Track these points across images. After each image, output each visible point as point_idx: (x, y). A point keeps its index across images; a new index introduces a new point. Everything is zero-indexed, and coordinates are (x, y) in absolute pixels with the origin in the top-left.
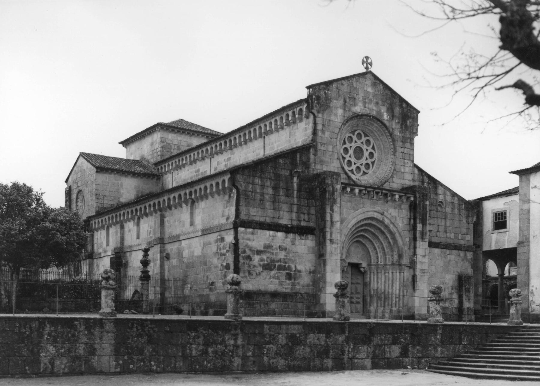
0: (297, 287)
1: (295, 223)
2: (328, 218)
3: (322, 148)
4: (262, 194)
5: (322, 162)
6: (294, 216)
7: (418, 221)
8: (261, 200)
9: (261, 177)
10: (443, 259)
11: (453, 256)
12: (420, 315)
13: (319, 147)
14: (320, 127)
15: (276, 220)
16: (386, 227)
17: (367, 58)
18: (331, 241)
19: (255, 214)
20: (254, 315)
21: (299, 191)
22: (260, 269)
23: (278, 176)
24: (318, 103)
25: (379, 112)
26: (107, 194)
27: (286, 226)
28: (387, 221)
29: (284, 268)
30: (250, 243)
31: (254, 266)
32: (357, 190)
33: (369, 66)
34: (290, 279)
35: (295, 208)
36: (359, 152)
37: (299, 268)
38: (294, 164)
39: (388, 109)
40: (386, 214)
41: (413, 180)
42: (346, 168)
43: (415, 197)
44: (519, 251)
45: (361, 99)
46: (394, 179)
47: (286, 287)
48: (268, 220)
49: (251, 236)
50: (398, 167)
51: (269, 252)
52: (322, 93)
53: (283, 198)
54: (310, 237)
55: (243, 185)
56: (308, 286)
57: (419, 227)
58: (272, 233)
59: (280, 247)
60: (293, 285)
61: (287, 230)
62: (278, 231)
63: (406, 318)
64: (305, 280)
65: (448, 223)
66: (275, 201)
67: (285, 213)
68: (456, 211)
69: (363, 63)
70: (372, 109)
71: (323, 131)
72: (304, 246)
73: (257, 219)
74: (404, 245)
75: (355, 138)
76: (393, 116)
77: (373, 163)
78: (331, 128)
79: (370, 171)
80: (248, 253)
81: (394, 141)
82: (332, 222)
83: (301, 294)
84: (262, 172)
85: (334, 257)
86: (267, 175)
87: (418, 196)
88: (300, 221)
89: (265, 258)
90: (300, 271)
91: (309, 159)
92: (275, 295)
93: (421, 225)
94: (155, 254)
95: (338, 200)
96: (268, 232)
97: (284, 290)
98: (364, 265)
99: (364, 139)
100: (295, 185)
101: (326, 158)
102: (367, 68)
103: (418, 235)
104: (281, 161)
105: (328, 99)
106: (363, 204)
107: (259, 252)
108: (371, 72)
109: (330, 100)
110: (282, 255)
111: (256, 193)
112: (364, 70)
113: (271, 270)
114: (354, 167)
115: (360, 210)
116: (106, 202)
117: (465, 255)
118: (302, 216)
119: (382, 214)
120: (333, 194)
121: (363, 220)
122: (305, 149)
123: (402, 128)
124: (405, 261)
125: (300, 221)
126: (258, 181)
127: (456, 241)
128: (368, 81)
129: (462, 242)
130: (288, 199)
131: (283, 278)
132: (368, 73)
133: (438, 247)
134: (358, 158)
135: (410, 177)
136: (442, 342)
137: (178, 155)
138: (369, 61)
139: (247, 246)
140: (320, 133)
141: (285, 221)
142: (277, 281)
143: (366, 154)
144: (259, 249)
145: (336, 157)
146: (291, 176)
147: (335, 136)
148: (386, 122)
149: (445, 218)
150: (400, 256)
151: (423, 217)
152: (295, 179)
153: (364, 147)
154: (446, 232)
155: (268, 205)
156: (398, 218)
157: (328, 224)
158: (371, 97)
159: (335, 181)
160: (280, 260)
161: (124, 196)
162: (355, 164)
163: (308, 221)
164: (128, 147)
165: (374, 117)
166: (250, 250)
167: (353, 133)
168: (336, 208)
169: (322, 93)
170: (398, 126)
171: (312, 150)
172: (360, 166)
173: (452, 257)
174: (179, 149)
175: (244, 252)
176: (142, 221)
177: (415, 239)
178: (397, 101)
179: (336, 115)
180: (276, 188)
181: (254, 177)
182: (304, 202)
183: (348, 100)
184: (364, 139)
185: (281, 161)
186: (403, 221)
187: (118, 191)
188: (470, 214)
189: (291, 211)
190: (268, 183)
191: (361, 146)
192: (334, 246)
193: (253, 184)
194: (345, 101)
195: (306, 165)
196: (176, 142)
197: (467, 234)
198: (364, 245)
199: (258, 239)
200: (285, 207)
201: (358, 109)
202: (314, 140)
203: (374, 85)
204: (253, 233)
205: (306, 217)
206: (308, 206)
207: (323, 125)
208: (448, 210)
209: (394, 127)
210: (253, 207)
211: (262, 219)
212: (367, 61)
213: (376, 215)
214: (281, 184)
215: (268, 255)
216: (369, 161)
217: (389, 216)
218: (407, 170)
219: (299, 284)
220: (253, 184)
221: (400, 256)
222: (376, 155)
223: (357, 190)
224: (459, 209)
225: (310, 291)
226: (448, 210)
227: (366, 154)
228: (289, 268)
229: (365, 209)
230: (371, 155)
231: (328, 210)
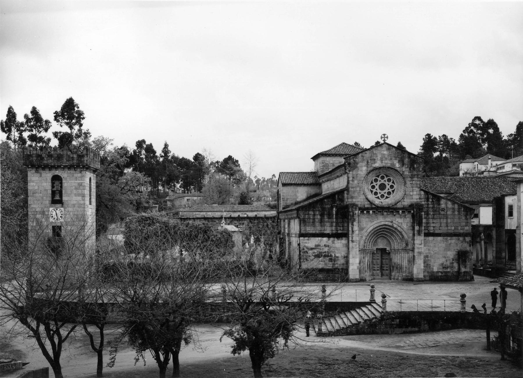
0: (336, 265)
1: (334, 232)
2: (350, 229)
3: (352, 190)
4: (314, 219)
5: (352, 198)
6: (334, 228)
7: (415, 224)
8: (313, 222)
9: (313, 211)
10: (445, 243)
11: (453, 241)
12: (417, 279)
13: (351, 189)
14: (351, 179)
15: (322, 232)
16: (396, 229)
18: (352, 241)
19: (310, 229)
21: (336, 215)
22: (313, 257)
23: (323, 209)
24: (349, 166)
25: (393, 164)
26: (289, 197)
27: (328, 234)
28: (395, 226)
29: (328, 256)
30: (306, 245)
31: (309, 256)
32: (371, 212)
33: (386, 139)
34: (331, 261)
35: (334, 224)
36: (382, 187)
37: (337, 255)
38: (334, 201)
39: (399, 161)
40: (394, 222)
41: (420, 198)
43: (414, 211)
44: (517, 232)
45: (379, 158)
46: (405, 200)
47: (330, 266)
48: (317, 232)
49: (307, 241)
50: (407, 193)
52: (352, 160)
53: (326, 220)
54: (344, 239)
55: (303, 216)
56: (343, 264)
57: (417, 228)
58: (320, 238)
59: (325, 245)
60: (334, 264)
61: (328, 236)
62: (323, 237)
65: (449, 221)
66: (321, 221)
67: (328, 228)
68: (456, 213)
70: (388, 163)
71: (353, 181)
72: (339, 244)
73: (311, 232)
74: (409, 238)
75: (379, 179)
76: (403, 164)
78: (358, 178)
79: (391, 196)
80: (306, 249)
81: (404, 178)
82: (353, 231)
83: (339, 269)
84: (314, 207)
85: (355, 250)
86: (317, 209)
87: (415, 210)
88: (337, 231)
89: (316, 251)
90: (338, 257)
91: (343, 197)
92: (321, 270)
93: (418, 227)
95: (357, 219)
96: (317, 238)
97: (328, 267)
98: (388, 249)
99: (386, 179)
100: (334, 212)
101: (356, 194)
102: (384, 140)
103: (416, 232)
104: (325, 200)
105: (356, 163)
106: (377, 218)
107: (312, 249)
109: (357, 164)
110: (326, 249)
111: (310, 219)
113: (320, 257)
115: (375, 222)
116: (288, 202)
117: (464, 239)
118: (339, 228)
119: (392, 222)
120: (353, 216)
121: (383, 225)
122: (341, 192)
123: (410, 170)
124: (410, 247)
125: (337, 231)
126: (311, 213)
127: (456, 231)
128: (385, 147)
129: (462, 231)
130: (330, 220)
131: (327, 262)
133: (441, 236)
135: (418, 197)
136: (325, 310)
137: (333, 170)
138: (386, 136)
139: (305, 246)
140: (351, 182)
141: (328, 231)
142: (324, 263)
145: (362, 193)
146: (332, 208)
147: (361, 182)
148: (398, 169)
149: (447, 218)
150: (407, 245)
151: (419, 221)
152: (334, 209)
153: (386, 183)
154: (447, 226)
155: (317, 224)
156: (403, 224)
157: (350, 232)
158: (386, 157)
159: (354, 209)
160: (325, 252)
161: (299, 198)
163: (343, 230)
164: (316, 161)
165: (389, 168)
168: (355, 223)
169: (352, 160)
170: (408, 169)
171: (345, 192)
173: (453, 241)
174: (333, 165)
175: (304, 249)
177: (414, 235)
178: (406, 155)
179: (361, 171)
180: (322, 215)
181: (309, 211)
182: (340, 220)
183: (370, 161)
184: (386, 179)
185: (325, 200)
186: (407, 225)
187: (296, 195)
188: (469, 213)
189: (332, 226)
190: (317, 213)
192: (354, 244)
193: (308, 214)
194: (368, 162)
195: (342, 200)
196: (331, 162)
197: (466, 226)
198: (386, 238)
199: (312, 242)
200: (328, 224)
201: (378, 164)
202: (347, 186)
203: (389, 149)
204: (308, 240)
205: (341, 228)
206: (343, 222)
207: (353, 178)
208: (449, 213)
209: (404, 170)
210: (308, 226)
211: (314, 232)
213: (387, 223)
214: (326, 213)
215: (317, 250)
217: (397, 223)
218: (415, 193)
219: (337, 264)
220: (308, 214)
221: (407, 245)
222: (395, 186)
223: (371, 212)
224: (459, 211)
225: (345, 268)
226: (449, 213)
228: (331, 256)
229: (378, 221)
230: (392, 187)
231: (350, 225)
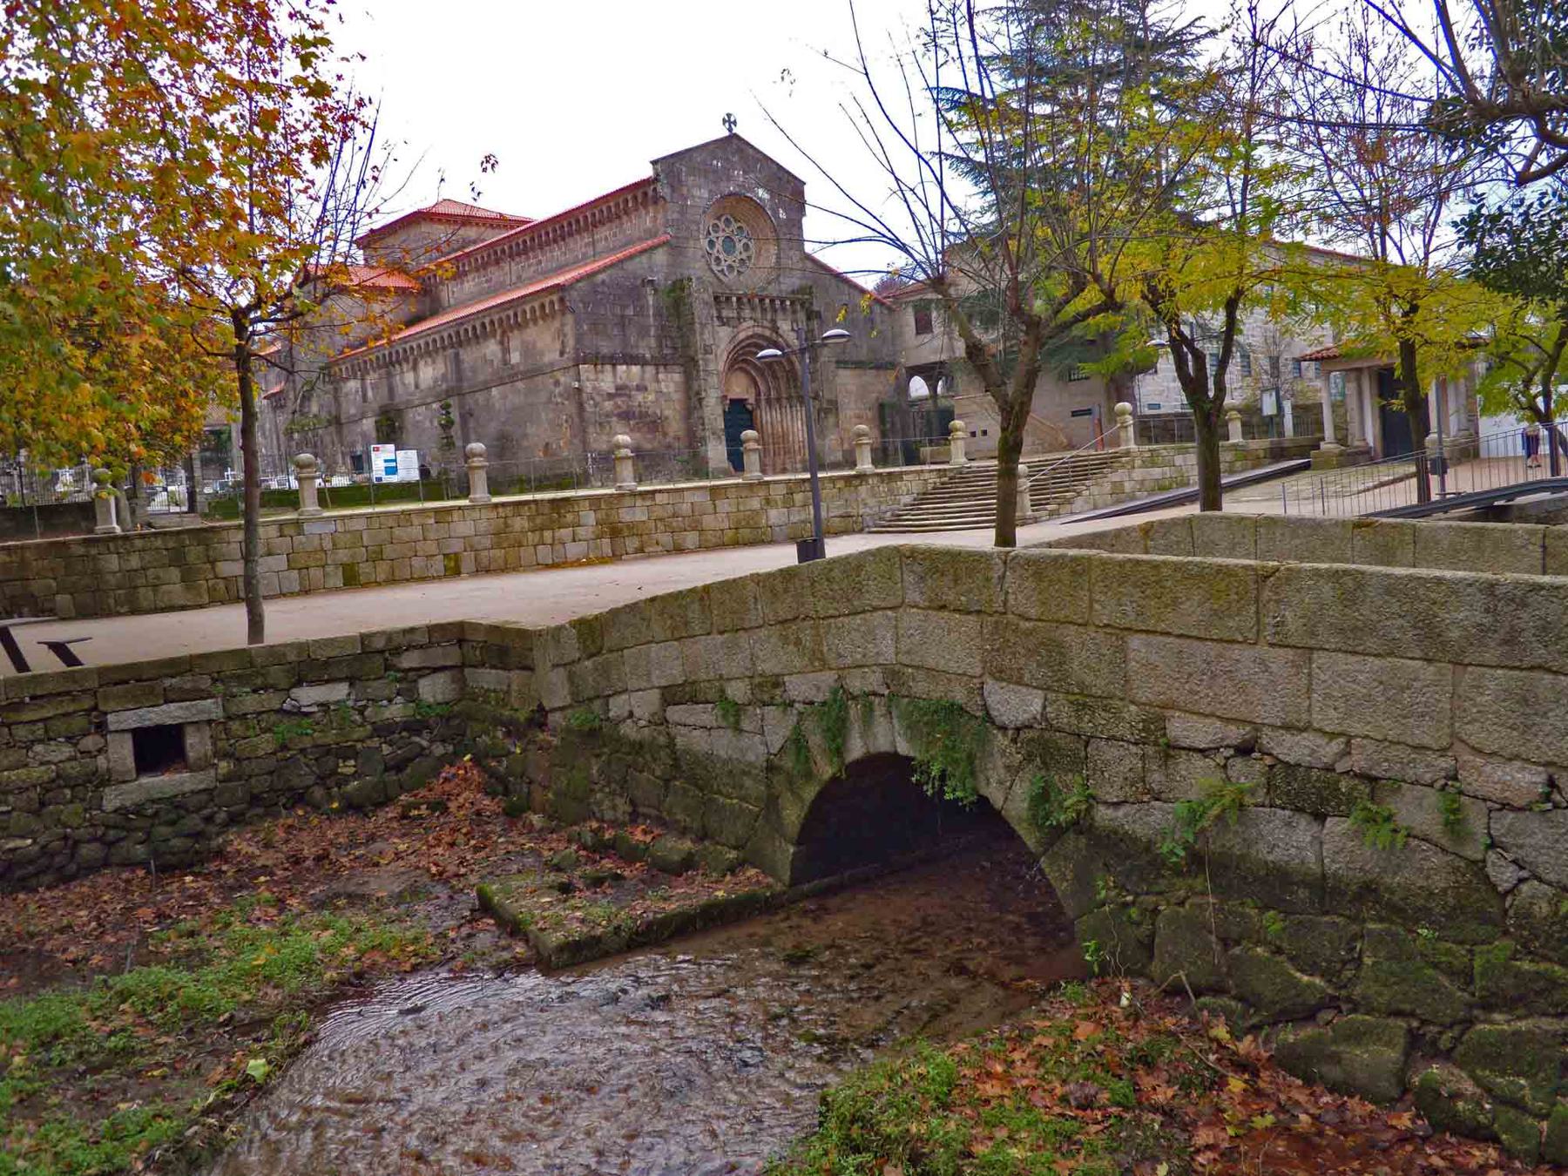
17: (729, 115)
20: (1074, 559)
42: (715, 268)
63: (449, 510)
64: (675, 427)
69: (724, 121)
77: (749, 258)
94: (1072, 698)
99: (735, 226)
102: (730, 130)
108: (736, 136)
112: (727, 133)
114: (724, 266)
132: (733, 138)
134: (728, 252)
143: (739, 246)
167: (719, 219)
176: (421, 364)
212: (729, 121)
216: (744, 256)
227: (739, 246)
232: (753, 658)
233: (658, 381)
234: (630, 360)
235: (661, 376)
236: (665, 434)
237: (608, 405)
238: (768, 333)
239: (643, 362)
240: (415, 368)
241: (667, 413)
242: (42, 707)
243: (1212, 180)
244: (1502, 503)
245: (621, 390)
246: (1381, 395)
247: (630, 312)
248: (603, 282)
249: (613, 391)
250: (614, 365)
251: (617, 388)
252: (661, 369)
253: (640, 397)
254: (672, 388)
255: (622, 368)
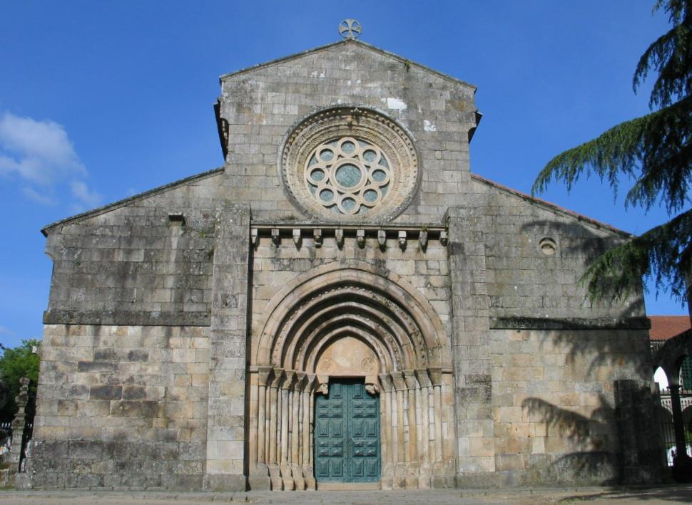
51: (106, 365)
90: (176, 399)
144: (85, 360)
162: (356, 156)
166: (66, 363)
172: (353, 196)
191: (342, 161)
222: (390, 174)
232: (517, 472)
233: (167, 346)
234: (124, 319)
235: (172, 341)
236: (169, 421)
237: (80, 379)
238: (367, 279)
239: (146, 321)
240: (107, 277)
241: (175, 391)
242: (381, 332)
243: (504, 379)
244: (689, 240)
245: (103, 358)
246: (628, 198)
247: (139, 257)
248: (105, 225)
249: (91, 359)
250: (98, 326)
251: (98, 356)
252: (176, 330)
253: (134, 368)
254: (190, 357)
255: (109, 331)
